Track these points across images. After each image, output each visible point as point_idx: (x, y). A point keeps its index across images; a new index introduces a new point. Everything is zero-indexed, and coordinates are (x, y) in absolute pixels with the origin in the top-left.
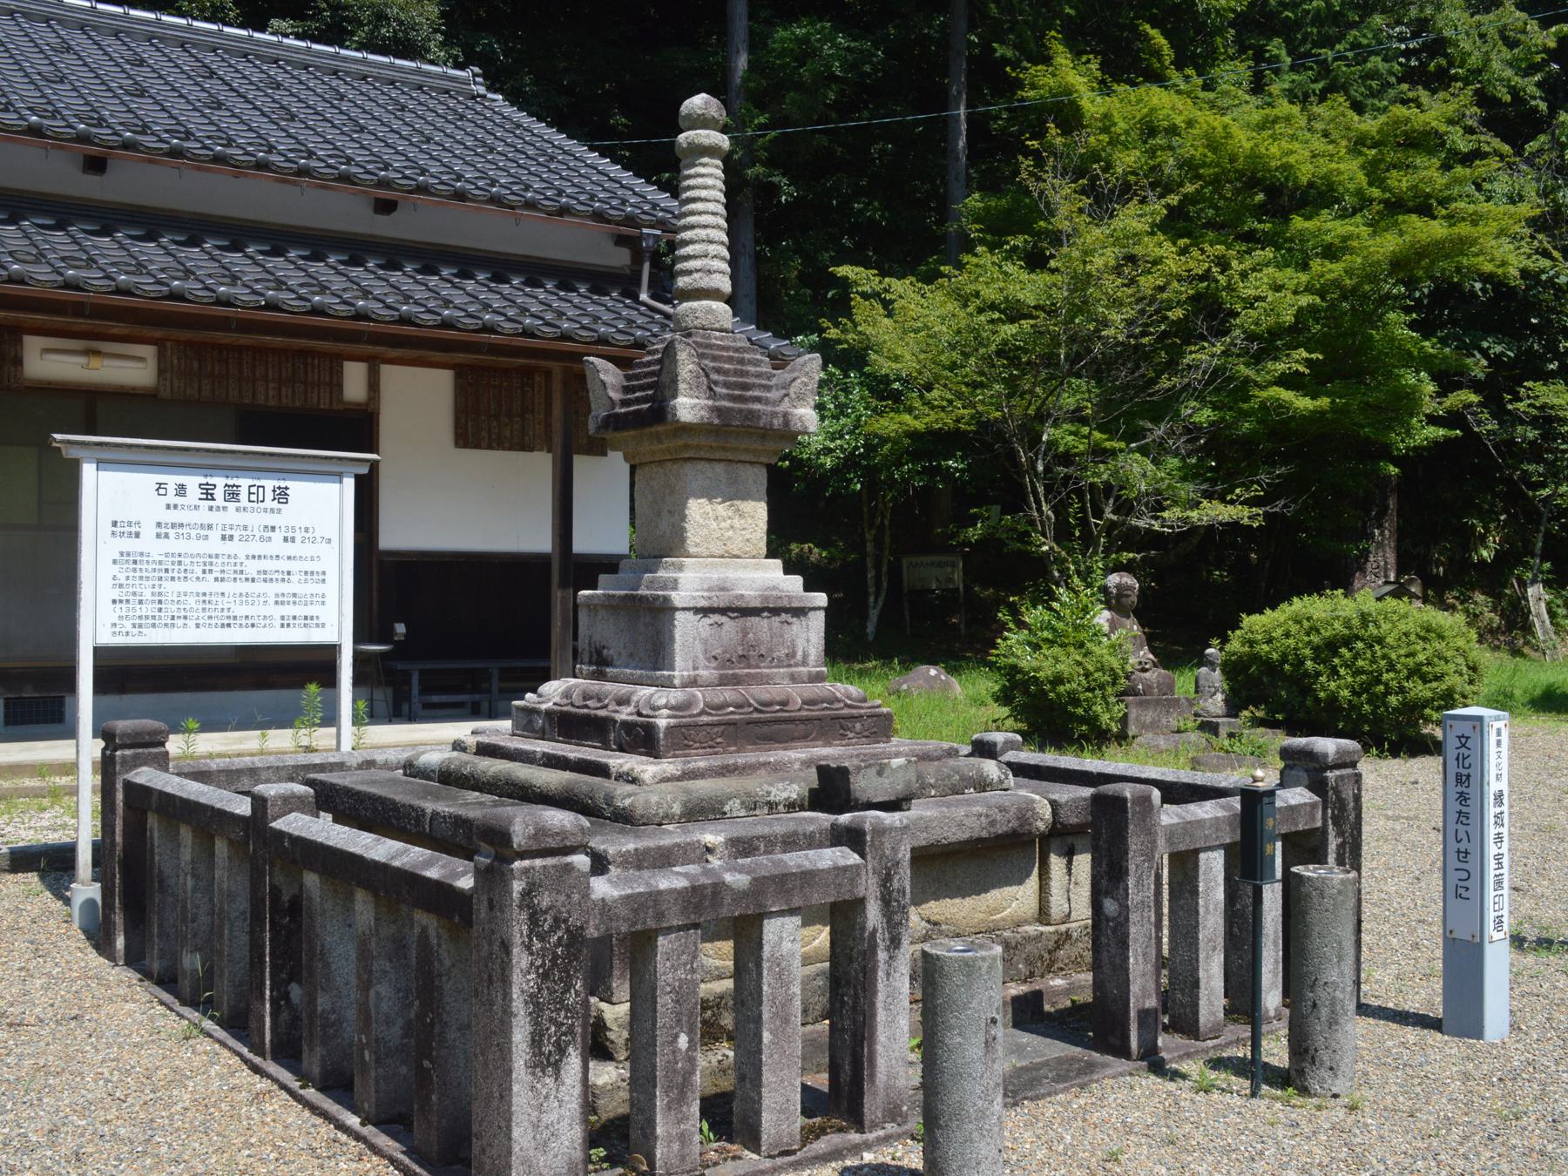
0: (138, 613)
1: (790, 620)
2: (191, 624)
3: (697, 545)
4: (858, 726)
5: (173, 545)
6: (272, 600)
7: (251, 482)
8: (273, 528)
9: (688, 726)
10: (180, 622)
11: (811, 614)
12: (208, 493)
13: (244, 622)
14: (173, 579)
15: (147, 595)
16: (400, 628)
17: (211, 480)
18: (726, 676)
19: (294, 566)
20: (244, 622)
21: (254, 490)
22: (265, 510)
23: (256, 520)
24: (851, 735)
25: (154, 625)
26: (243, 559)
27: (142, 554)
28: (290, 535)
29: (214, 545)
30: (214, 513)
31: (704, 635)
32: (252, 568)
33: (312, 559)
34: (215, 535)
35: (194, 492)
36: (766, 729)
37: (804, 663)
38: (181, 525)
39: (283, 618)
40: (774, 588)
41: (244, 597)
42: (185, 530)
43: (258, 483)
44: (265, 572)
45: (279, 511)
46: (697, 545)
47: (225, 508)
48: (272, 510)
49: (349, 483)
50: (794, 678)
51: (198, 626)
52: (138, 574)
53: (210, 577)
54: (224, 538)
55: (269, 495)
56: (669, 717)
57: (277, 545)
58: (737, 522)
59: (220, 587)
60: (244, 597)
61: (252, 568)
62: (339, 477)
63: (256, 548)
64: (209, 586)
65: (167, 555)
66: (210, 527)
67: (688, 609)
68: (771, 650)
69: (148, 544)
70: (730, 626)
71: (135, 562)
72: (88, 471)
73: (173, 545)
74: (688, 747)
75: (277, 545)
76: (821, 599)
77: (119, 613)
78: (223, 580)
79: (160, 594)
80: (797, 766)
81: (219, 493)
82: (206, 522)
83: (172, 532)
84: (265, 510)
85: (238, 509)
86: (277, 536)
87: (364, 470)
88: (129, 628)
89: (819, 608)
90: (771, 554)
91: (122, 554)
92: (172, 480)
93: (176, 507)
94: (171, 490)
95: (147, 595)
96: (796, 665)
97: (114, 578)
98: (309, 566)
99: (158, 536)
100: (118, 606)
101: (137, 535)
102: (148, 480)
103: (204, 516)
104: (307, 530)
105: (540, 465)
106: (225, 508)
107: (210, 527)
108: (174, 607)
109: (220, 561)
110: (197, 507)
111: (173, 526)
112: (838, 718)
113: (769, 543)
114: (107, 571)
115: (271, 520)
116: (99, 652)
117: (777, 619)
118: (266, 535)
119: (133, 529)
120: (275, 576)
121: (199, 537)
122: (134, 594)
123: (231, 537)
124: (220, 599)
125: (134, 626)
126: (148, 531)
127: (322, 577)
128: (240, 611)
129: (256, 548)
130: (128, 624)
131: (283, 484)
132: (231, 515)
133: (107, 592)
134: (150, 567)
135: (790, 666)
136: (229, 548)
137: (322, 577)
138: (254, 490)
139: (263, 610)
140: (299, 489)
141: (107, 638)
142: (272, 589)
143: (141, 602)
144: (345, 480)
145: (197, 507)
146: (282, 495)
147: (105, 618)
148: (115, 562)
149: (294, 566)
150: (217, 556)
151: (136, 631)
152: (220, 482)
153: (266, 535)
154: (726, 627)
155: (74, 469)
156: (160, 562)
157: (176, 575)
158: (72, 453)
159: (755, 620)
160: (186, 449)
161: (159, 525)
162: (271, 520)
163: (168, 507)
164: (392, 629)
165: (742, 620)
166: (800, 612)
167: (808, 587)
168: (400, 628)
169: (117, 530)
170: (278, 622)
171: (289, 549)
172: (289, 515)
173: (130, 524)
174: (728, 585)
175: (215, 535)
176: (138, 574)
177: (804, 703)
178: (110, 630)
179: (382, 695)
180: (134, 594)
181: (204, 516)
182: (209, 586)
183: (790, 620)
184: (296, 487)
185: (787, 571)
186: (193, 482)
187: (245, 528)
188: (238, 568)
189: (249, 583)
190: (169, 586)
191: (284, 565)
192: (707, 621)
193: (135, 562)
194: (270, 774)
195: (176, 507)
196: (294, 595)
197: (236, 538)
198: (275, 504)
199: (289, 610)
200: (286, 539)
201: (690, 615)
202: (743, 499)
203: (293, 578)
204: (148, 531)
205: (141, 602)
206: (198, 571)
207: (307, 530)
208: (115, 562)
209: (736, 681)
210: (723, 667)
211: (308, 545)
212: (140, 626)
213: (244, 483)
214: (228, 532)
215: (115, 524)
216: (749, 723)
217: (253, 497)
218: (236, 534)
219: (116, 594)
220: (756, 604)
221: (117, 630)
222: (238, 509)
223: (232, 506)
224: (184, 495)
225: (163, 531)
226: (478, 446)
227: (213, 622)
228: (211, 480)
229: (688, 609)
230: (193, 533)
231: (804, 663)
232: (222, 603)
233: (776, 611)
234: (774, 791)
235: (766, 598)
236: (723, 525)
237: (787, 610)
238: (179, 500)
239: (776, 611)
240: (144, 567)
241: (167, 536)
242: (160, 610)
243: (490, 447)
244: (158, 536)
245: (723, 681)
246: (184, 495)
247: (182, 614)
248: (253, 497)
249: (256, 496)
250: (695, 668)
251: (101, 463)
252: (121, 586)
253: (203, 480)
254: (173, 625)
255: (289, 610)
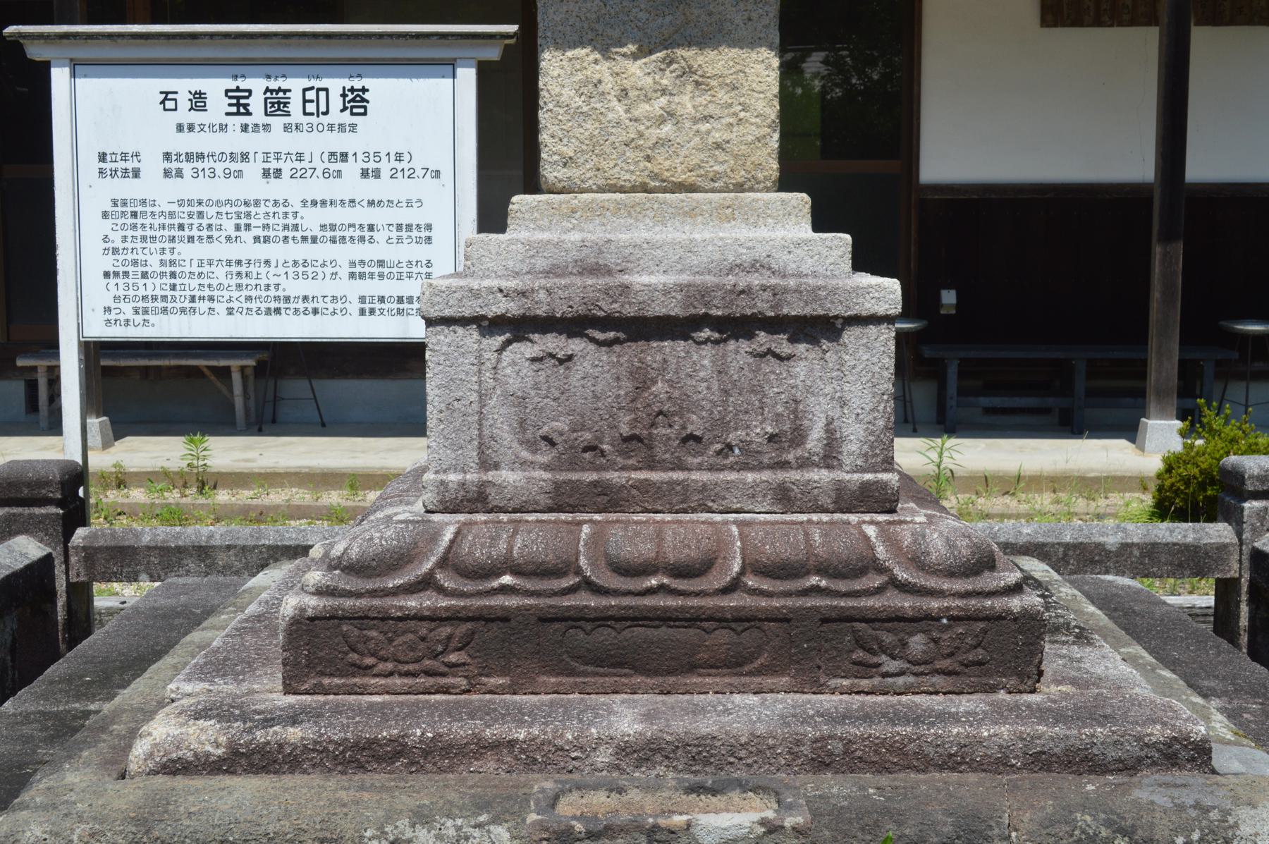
0: (141, 292)
1: (785, 348)
2: (221, 308)
3: (567, 162)
4: (917, 643)
5: (190, 187)
6: (344, 271)
7: (306, 83)
8: (344, 156)
9: (361, 618)
10: (204, 306)
11: (850, 335)
12: (239, 103)
13: (301, 306)
14: (191, 239)
15: (154, 264)
16: (949, 297)
17: (243, 84)
18: (575, 486)
19: (379, 216)
20: (301, 306)
21: (311, 95)
22: (331, 127)
23: (316, 144)
24: (892, 665)
25: (165, 311)
26: (297, 206)
27: (143, 202)
28: (371, 165)
29: (252, 185)
30: (251, 135)
31: (514, 384)
32: (312, 220)
33: (409, 204)
34: (253, 170)
35: (218, 104)
36: (605, 636)
37: (830, 457)
38: (201, 156)
39: (362, 299)
40: (755, 266)
41: (301, 267)
42: (207, 164)
43: (318, 84)
44: (333, 227)
45: (353, 127)
46: (567, 162)
47: (267, 127)
48: (342, 128)
49: (467, 77)
50: (785, 498)
51: (230, 312)
52: (139, 233)
53: (247, 236)
54: (266, 173)
55: (337, 103)
56: (320, 592)
57: (350, 183)
58: (687, 102)
59: (262, 251)
60: (301, 267)
61: (312, 220)
62: (448, 66)
63: (317, 188)
64: (246, 249)
65: (180, 203)
66: (245, 157)
67: (463, 322)
68: (722, 424)
69: (153, 186)
70: (594, 365)
71: (134, 214)
72: (59, 77)
73: (190, 187)
74: (366, 670)
75: (350, 183)
76: (884, 292)
77: (113, 291)
78: (266, 240)
79: (173, 263)
80: (603, 757)
81: (256, 103)
82: (237, 150)
83: (187, 167)
84: (331, 127)
85: (287, 128)
86: (351, 169)
87: (493, 53)
88: (129, 314)
89: (874, 320)
90: (786, 183)
91: (115, 202)
92: (184, 86)
93: (191, 127)
94: (184, 101)
95: (154, 264)
96: (804, 464)
97: (106, 239)
98: (405, 216)
99: (167, 173)
100: (112, 281)
101: (136, 173)
102: (149, 87)
103: (234, 140)
104: (399, 157)
105: (1139, 47)
106: (267, 127)
107: (245, 157)
108: (195, 283)
109: (262, 209)
110: (223, 127)
111: (189, 157)
112: (847, 618)
113: (785, 155)
114: (95, 229)
115: (339, 142)
116: (93, 351)
117: (744, 345)
118: (333, 167)
119: (130, 165)
120: (347, 234)
121: (228, 174)
122: (135, 263)
123: (278, 173)
124: (263, 270)
125: (136, 311)
126: (152, 166)
127: (425, 233)
128: (295, 288)
129: (317, 188)
130: (127, 308)
131: (358, 84)
132: (277, 138)
133: (96, 262)
134: (156, 222)
135: (784, 465)
136: (275, 189)
137: (425, 233)
138: (311, 95)
139: (331, 288)
140: (384, 90)
141: (97, 330)
142: (344, 254)
143: (145, 275)
144: (460, 71)
145: (223, 127)
146: (356, 102)
147: (93, 300)
148: (105, 215)
149: (379, 216)
150: (257, 203)
151: (139, 319)
152: (257, 85)
153: (333, 167)
154: (582, 368)
155: (42, 72)
156: (172, 215)
157: (195, 233)
158: (35, 52)
159: (672, 349)
160: (194, 36)
161: (167, 156)
162: (339, 142)
163: (180, 128)
164: (938, 298)
165: (632, 349)
166: (820, 328)
167: (861, 262)
168: (949, 297)
169: (108, 166)
170: (354, 307)
171: (371, 188)
172: (369, 134)
173: (124, 156)
174: (611, 259)
175: (253, 170)
176: (139, 233)
177: (753, 566)
178: (101, 317)
179: (923, 394)
180: (135, 263)
181: (234, 140)
182: (246, 249)
183: (785, 348)
184: (380, 88)
185: (821, 222)
186: (215, 87)
187: (300, 156)
188: (291, 221)
189: (308, 246)
190: (187, 252)
191: (363, 215)
192: (524, 350)
193: (134, 214)
194: (231, 558)
195: (191, 127)
196: (381, 263)
197: (286, 173)
198: (346, 118)
199: (373, 288)
200: (365, 174)
201: (470, 337)
202: (705, 40)
203: (380, 236)
204: (152, 166)
205: (145, 275)
206: (229, 226)
207: (399, 157)
208: (105, 215)
209: (609, 499)
210: (573, 465)
211: (401, 181)
212: (145, 311)
213: (295, 85)
214: (273, 165)
215: (103, 157)
216: (546, 619)
217: (311, 108)
218: (286, 167)
219: (108, 263)
220: (674, 308)
221: (112, 317)
222: (287, 128)
223: (277, 122)
224: (203, 109)
225: (174, 165)
226: (1077, 22)
227: (254, 305)
228: (243, 84)
229: (463, 322)
230: (220, 167)
231: (830, 457)
232: (267, 276)
233: (736, 327)
234: (603, 798)
235: (703, 293)
236: (643, 109)
237: (775, 324)
238: (196, 117)
239: (736, 327)
240: (148, 221)
241: (179, 173)
242: (173, 287)
243: (1098, 23)
244: (167, 173)
245: (564, 500)
246: (203, 109)
247: (207, 293)
248: (311, 108)
249: (315, 105)
250: (486, 464)
251: (77, 67)
252: (115, 251)
253: (231, 84)
254: (193, 310)
255: (373, 288)
